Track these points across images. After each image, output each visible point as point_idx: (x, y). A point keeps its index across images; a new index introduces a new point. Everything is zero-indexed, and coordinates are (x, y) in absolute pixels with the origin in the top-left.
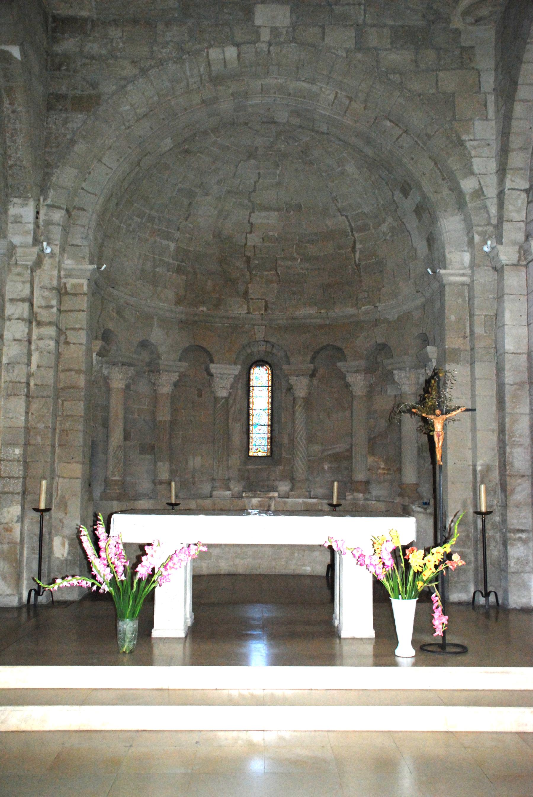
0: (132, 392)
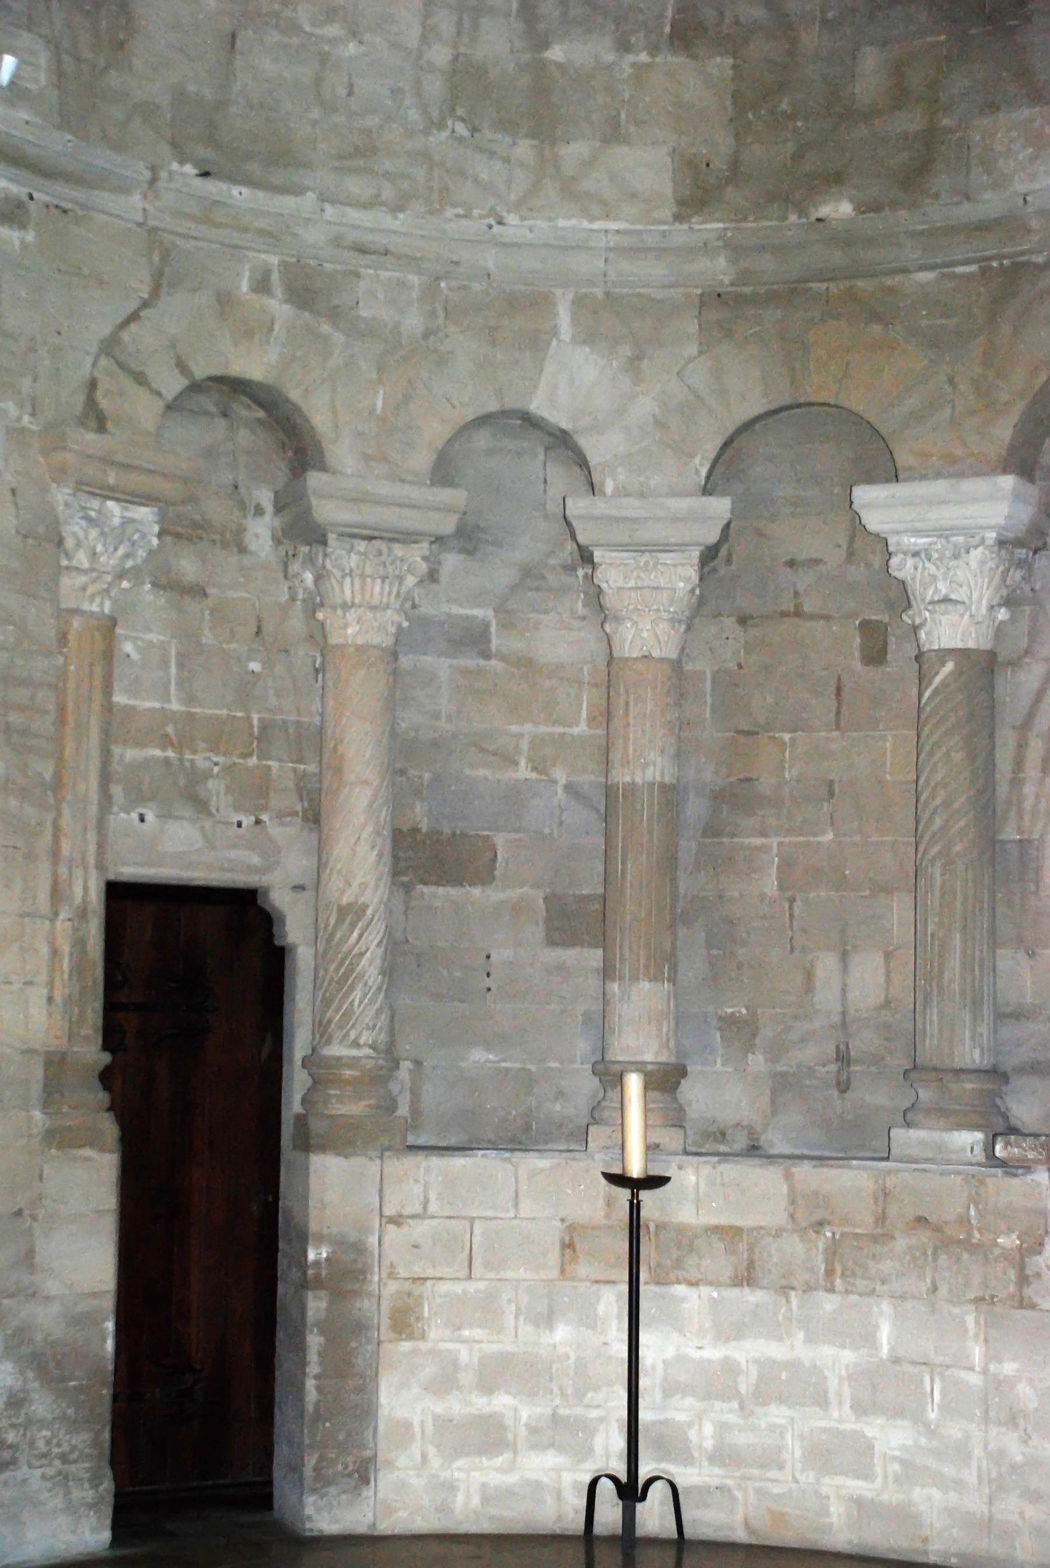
0: (495, 664)
